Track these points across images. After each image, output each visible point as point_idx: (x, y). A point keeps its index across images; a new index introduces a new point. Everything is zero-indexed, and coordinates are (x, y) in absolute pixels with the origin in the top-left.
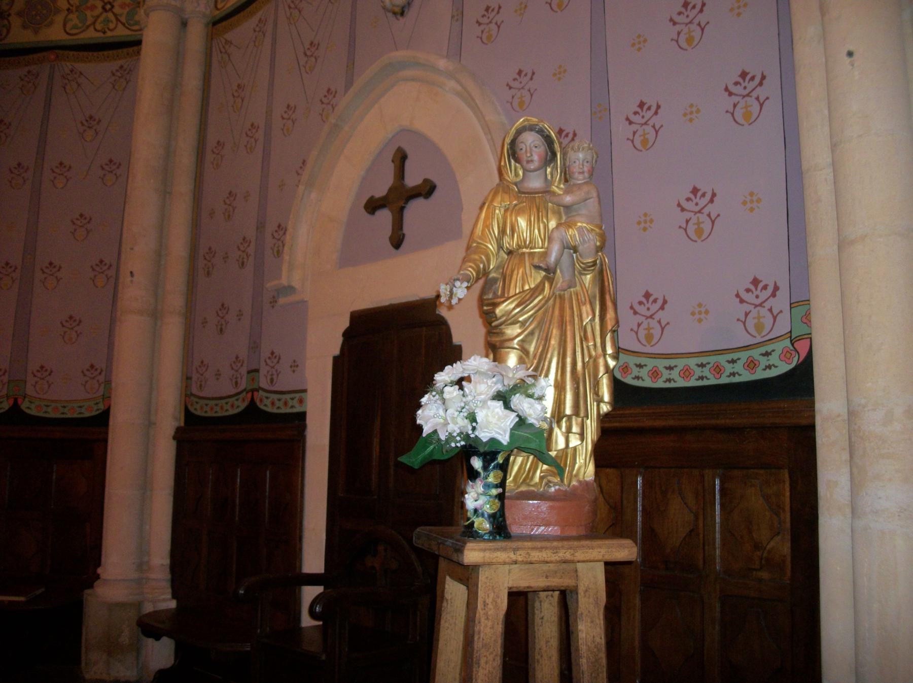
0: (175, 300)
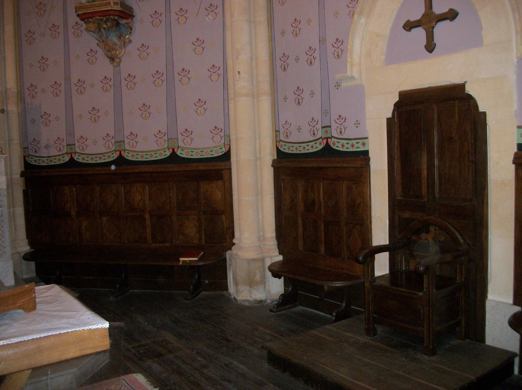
0: (266, 87)
